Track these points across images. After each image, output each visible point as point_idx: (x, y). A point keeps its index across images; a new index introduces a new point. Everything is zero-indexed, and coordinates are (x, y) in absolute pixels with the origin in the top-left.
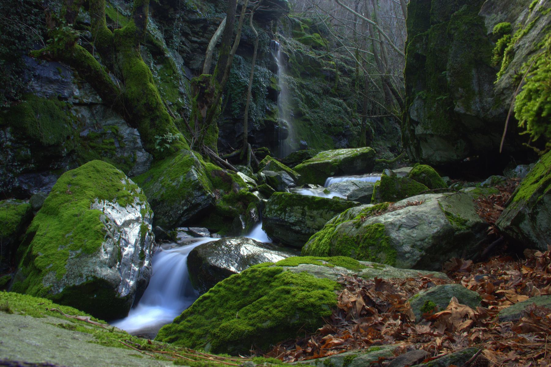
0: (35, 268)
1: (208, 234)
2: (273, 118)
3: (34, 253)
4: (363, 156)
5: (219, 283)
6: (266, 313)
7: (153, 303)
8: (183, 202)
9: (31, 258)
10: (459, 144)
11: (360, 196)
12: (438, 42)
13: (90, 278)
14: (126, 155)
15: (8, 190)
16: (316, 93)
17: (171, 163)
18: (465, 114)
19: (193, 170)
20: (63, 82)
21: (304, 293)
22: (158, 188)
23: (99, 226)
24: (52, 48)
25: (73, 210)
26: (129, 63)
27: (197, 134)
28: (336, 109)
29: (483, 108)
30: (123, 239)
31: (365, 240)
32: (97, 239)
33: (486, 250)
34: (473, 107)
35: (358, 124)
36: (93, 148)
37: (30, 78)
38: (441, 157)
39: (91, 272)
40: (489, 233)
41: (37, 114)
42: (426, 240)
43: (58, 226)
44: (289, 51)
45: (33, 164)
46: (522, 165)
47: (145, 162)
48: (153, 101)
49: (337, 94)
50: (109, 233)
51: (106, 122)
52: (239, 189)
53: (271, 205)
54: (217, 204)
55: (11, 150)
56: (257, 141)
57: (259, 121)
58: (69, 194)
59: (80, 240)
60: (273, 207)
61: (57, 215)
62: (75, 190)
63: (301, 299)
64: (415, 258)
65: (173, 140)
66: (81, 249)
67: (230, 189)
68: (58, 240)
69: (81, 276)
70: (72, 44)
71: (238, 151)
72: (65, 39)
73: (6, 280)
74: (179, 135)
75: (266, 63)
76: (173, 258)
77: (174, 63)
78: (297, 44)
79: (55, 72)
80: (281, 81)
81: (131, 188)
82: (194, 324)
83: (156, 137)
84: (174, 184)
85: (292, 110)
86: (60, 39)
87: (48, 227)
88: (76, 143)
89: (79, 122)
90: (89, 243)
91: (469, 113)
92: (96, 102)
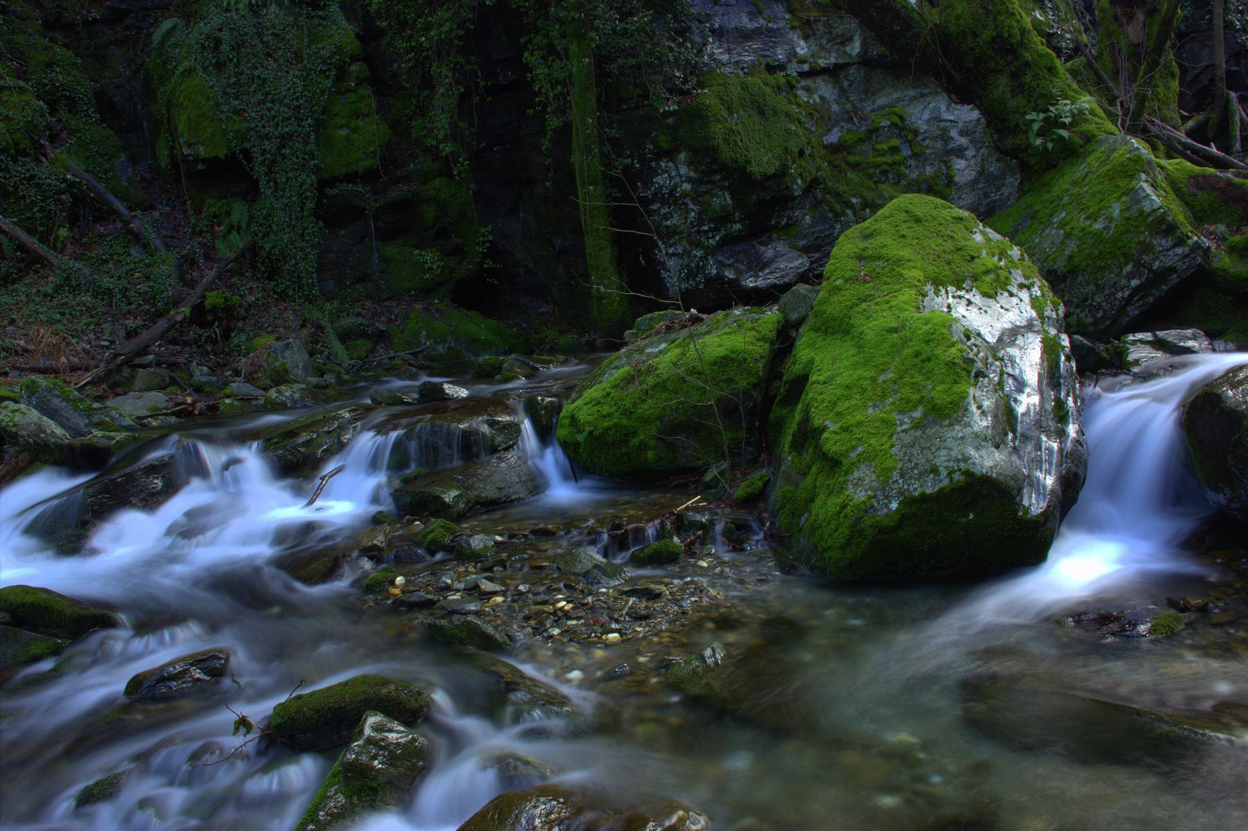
0: (824, 456)
1: (1205, 343)
3: (817, 422)
7: (1096, 527)
8: (1129, 268)
9: (808, 435)
13: (957, 476)
14: (929, 171)
15: (698, 284)
17: (1078, 175)
19: (1145, 185)
20: (770, 30)
22: (1057, 241)
23: (953, 350)
25: (887, 319)
30: (1010, 375)
32: (956, 382)
36: (855, 166)
37: (704, 38)
39: (958, 461)
47: (975, 182)
48: (1011, 27)
50: (979, 365)
54: (1215, 265)
55: (693, 200)
58: (866, 282)
61: (847, 332)
62: (878, 270)
65: (1073, 115)
66: (920, 408)
68: (865, 390)
69: (935, 471)
71: (1200, 117)
73: (760, 483)
74: (1087, 101)
79: (750, 13)
81: (997, 251)
83: (1028, 117)
84: (1098, 226)
87: (834, 361)
88: (818, 161)
89: (816, 115)
90: (939, 393)
92: (847, 60)
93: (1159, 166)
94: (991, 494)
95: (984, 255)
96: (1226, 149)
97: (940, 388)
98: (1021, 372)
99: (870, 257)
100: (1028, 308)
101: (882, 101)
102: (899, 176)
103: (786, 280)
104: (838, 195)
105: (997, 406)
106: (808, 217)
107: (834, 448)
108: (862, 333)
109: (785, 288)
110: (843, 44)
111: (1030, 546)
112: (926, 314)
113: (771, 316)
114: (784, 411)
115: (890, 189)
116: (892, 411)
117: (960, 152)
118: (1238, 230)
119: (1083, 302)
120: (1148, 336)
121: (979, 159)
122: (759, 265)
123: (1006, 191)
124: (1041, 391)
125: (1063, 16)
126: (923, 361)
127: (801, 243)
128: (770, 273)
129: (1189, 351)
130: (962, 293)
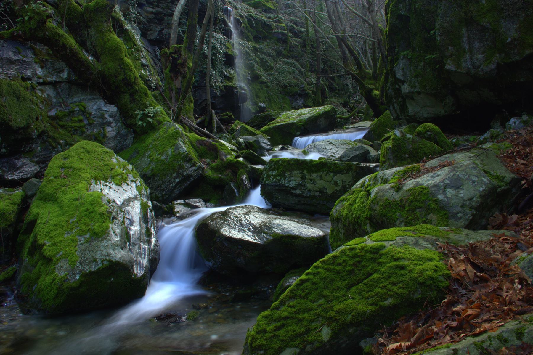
1: (203, 203)
2: (232, 83)
3: (40, 242)
4: (326, 114)
5: (315, 264)
6: (385, 291)
7: (164, 279)
8: (175, 175)
9: (36, 248)
10: (447, 101)
11: (351, 156)
12: (425, 2)
13: (105, 263)
14: (96, 131)
16: (270, 56)
17: (156, 137)
18: (456, 72)
19: (180, 142)
20: (24, 61)
21: (419, 267)
22: (147, 163)
23: (103, 208)
24: (22, 27)
26: (103, 39)
27: (175, 107)
28: (290, 70)
29: (473, 65)
31: (410, 203)
32: (104, 222)
33: (522, 203)
34: (464, 65)
35: (312, 83)
36: (62, 127)
38: (428, 113)
39: (106, 256)
40: (523, 187)
41: (3, 97)
42: (474, 199)
43: (59, 212)
44: (241, 16)
45: (4, 148)
46: (516, 118)
47: (115, 137)
48: (130, 75)
49: (289, 55)
50: (114, 214)
51: (72, 99)
52: (226, 157)
53: (268, 171)
54: (207, 174)
56: (218, 107)
57: (219, 87)
58: (64, 178)
59: (85, 223)
60: (270, 173)
61: (55, 201)
62: (70, 173)
63: (419, 274)
64: (467, 217)
65: (154, 113)
67: (216, 158)
68: (63, 226)
69: (95, 261)
70: (44, 22)
72: (36, 17)
73: (12, 272)
74: (159, 108)
75: (220, 29)
76: (178, 232)
77: (133, 35)
78: (247, 9)
79: (14, 52)
80: (236, 45)
81: (122, 166)
82: (300, 309)
83: (136, 113)
84: (163, 158)
85: (249, 74)
86: (31, 18)
87: (49, 213)
89: (45, 102)
90: (97, 227)
91: (459, 70)
92: (60, 80)
93: (186, 135)
94: (119, 270)
95: (117, 168)
96: (211, 132)
97: (97, 224)
98: (132, 217)
99: (67, 167)
100: (135, 191)
101: (76, 99)
102: (82, 133)
103: (28, 176)
104: (54, 139)
105: (122, 232)
106: (39, 148)
107: (49, 253)
108: (62, 201)
109: (27, 180)
110: (59, 72)
111: (137, 290)
112: (91, 192)
113: (18, 193)
114: (25, 237)
115: (78, 138)
116: (76, 235)
117: (109, 124)
118: (214, 161)
119: (157, 188)
120: (182, 202)
121: (117, 127)
122: (14, 169)
123: (128, 141)
124: (140, 225)
125: (153, 73)
126: (89, 213)
127: (36, 159)
128: (20, 173)
129: (197, 207)
130: (107, 184)
